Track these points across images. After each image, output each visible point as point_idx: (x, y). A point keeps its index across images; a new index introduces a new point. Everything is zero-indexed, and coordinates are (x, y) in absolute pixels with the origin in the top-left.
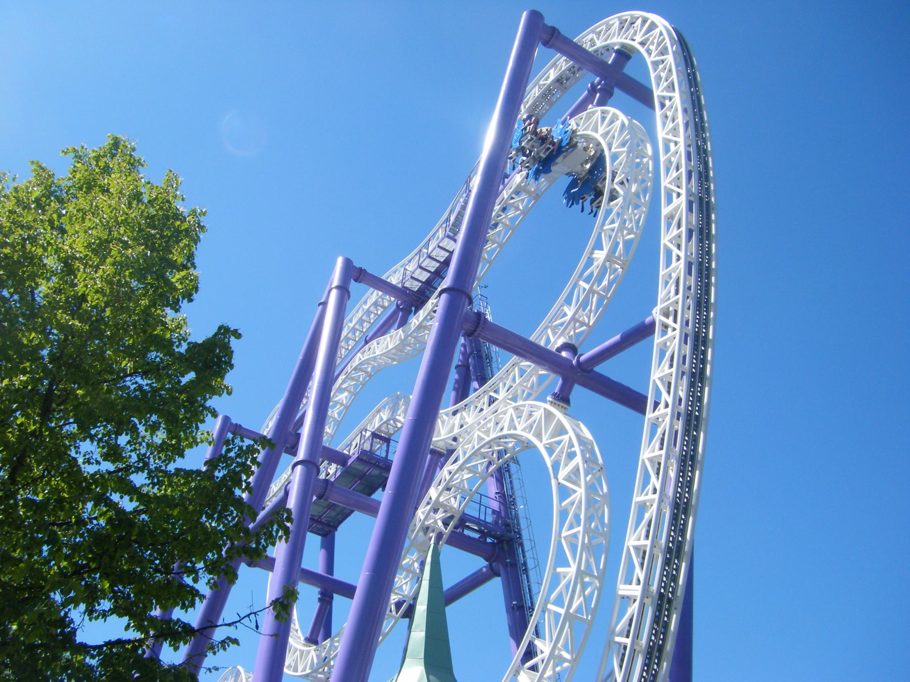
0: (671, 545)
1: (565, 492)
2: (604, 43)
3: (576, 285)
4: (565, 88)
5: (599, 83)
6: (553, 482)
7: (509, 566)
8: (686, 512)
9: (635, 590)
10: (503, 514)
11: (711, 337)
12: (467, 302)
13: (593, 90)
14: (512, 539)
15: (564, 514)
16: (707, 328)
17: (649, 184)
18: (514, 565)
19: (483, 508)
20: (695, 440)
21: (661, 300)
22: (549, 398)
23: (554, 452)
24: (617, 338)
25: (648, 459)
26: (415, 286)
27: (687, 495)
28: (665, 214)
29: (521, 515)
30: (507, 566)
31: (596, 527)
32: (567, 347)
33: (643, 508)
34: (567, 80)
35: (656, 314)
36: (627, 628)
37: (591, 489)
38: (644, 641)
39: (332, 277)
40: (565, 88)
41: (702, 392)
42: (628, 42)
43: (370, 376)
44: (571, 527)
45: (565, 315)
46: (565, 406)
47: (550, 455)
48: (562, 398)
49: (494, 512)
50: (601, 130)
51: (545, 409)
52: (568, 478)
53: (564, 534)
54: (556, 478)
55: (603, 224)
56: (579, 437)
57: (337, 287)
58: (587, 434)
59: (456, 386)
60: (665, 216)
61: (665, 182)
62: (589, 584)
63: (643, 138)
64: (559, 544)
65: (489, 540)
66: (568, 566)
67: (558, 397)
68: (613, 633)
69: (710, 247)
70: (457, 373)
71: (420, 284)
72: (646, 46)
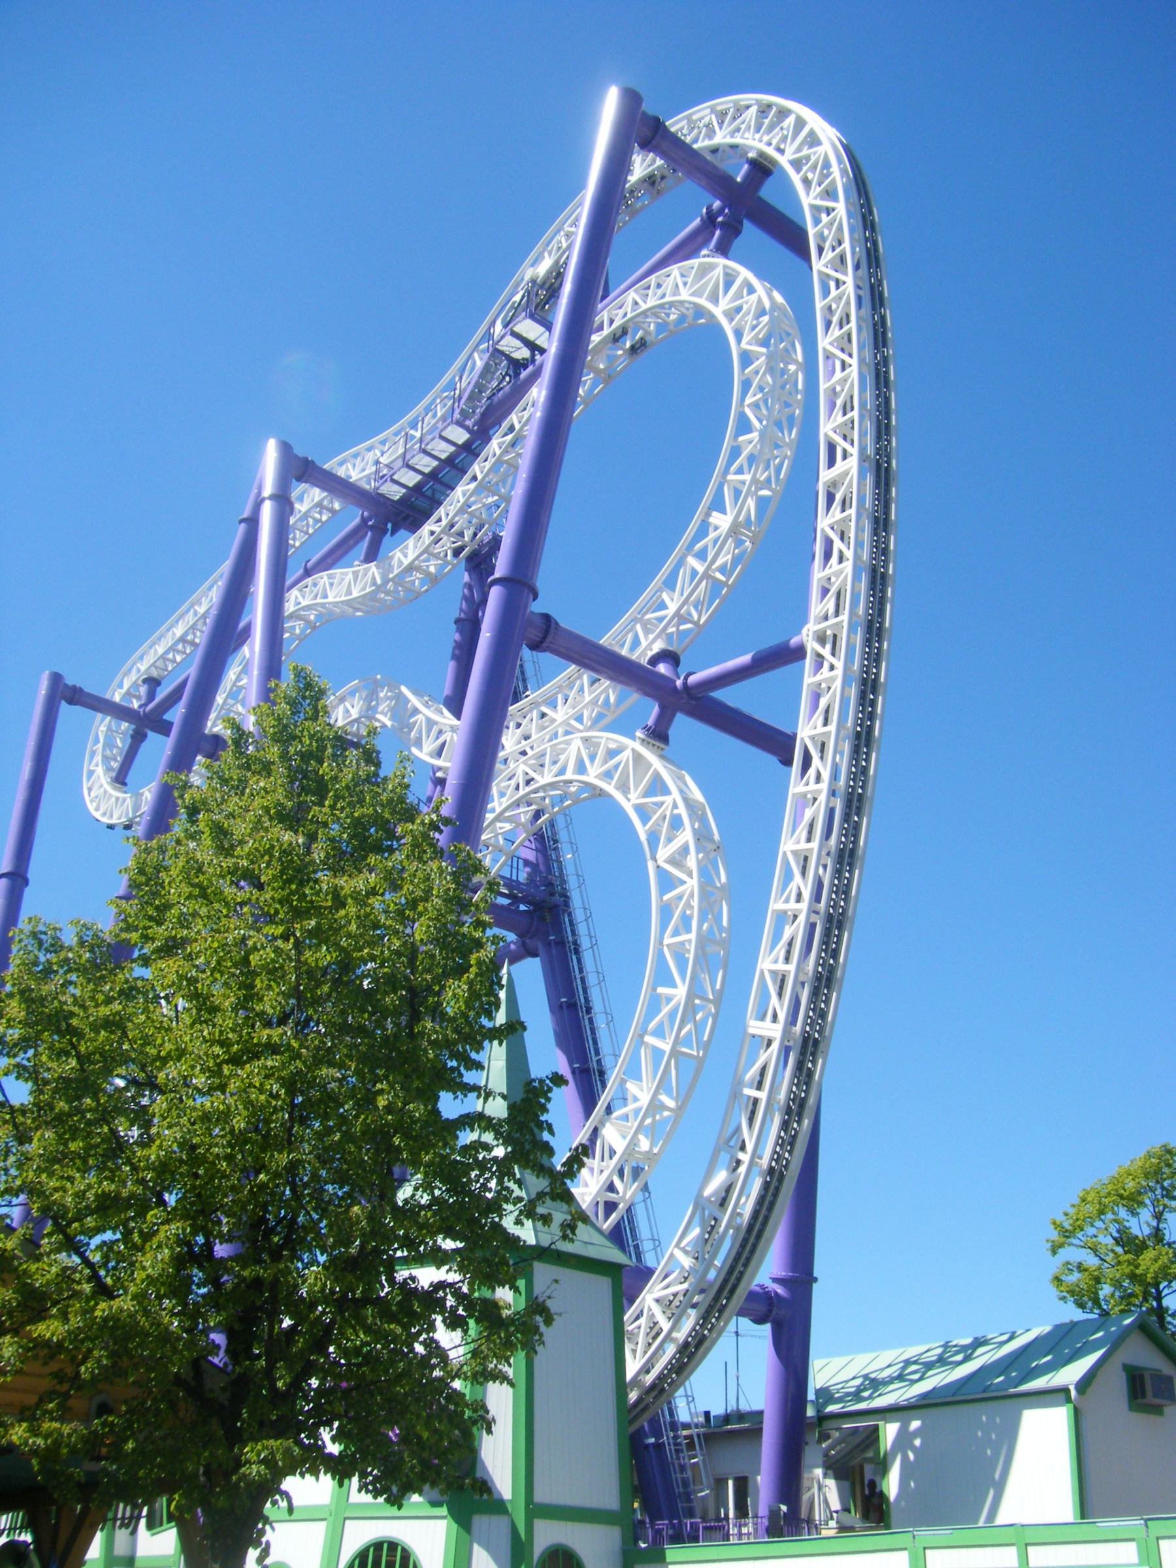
0: (820, 969)
1: (667, 882)
2: (729, 140)
3: (681, 562)
4: (658, 192)
5: (720, 212)
6: (651, 865)
7: (553, 945)
8: (840, 927)
9: (775, 1031)
10: (542, 867)
11: (882, 680)
12: (531, 597)
13: (710, 220)
14: (556, 906)
15: (666, 912)
16: (878, 667)
17: (797, 412)
18: (561, 943)
19: (515, 859)
20: (857, 827)
21: (816, 617)
22: (639, 734)
23: (650, 818)
24: (745, 659)
25: (793, 852)
26: (395, 493)
27: (842, 903)
28: (826, 479)
29: (569, 870)
30: (549, 944)
31: (710, 930)
32: (664, 656)
33: (783, 918)
34: (663, 178)
35: (807, 636)
36: (758, 1078)
37: (706, 874)
38: (782, 1096)
39: (258, 476)
40: (658, 192)
41: (867, 760)
42: (771, 151)
43: (314, 628)
44: (676, 933)
45: (663, 606)
46: (662, 746)
47: (644, 822)
48: (659, 735)
49: (527, 863)
50: (725, 303)
51: (633, 750)
52: (671, 861)
53: (667, 941)
54: (654, 859)
55: (726, 471)
56: (686, 800)
57: (272, 497)
58: (697, 794)
59: (457, 652)
60: (825, 483)
61: (828, 427)
62: (702, 1008)
63: (790, 331)
64: (660, 956)
65: (522, 907)
66: (674, 986)
67: (653, 732)
68: (738, 1083)
69: (887, 543)
70: (457, 631)
71: (404, 491)
72: (802, 173)
